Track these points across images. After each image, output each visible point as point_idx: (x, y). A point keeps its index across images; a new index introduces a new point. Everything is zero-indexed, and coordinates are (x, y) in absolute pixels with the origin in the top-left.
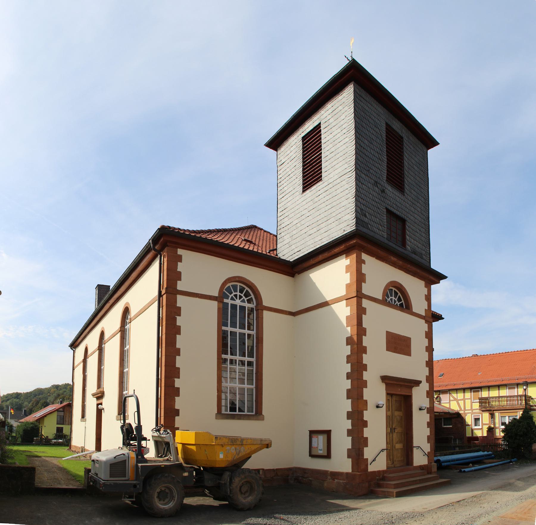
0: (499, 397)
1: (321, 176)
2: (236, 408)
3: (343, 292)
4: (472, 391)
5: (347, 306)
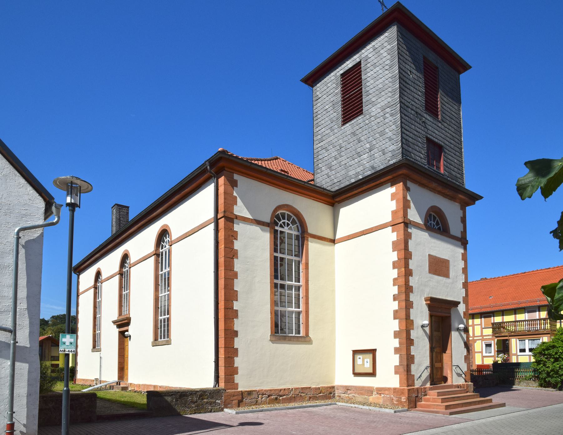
0: (516, 321)
1: (362, 110)
4: (483, 317)
5: (239, 225)
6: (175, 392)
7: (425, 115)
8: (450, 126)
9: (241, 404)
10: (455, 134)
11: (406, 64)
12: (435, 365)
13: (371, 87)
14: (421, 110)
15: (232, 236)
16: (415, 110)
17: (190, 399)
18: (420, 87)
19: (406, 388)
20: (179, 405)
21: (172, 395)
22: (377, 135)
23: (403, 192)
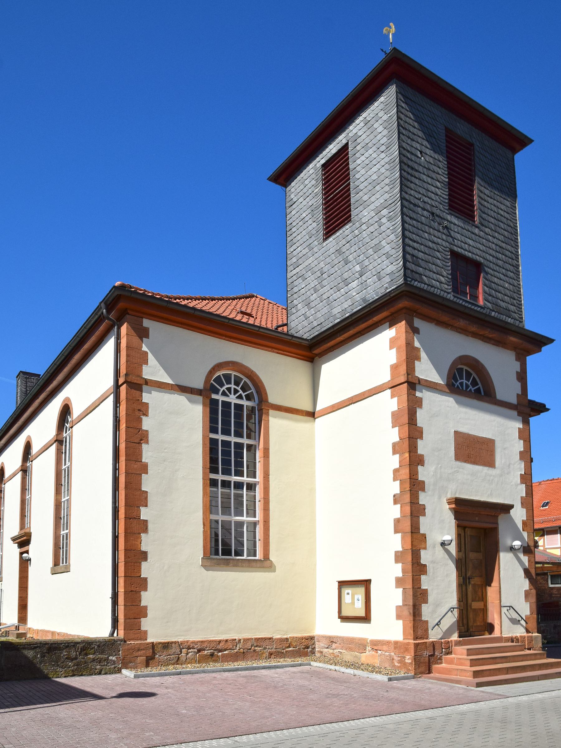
1: (350, 216)
2: (231, 550)
3: (385, 377)
5: (151, 393)
6: (41, 644)
7: (449, 217)
8: (496, 232)
9: (151, 662)
10: (506, 244)
11: (414, 140)
12: (473, 605)
13: (362, 179)
14: (441, 210)
15: (139, 410)
16: (430, 211)
17: (65, 653)
18: (439, 174)
19: (412, 641)
20: (47, 663)
21: (35, 648)
22: (371, 251)
23: (406, 336)
